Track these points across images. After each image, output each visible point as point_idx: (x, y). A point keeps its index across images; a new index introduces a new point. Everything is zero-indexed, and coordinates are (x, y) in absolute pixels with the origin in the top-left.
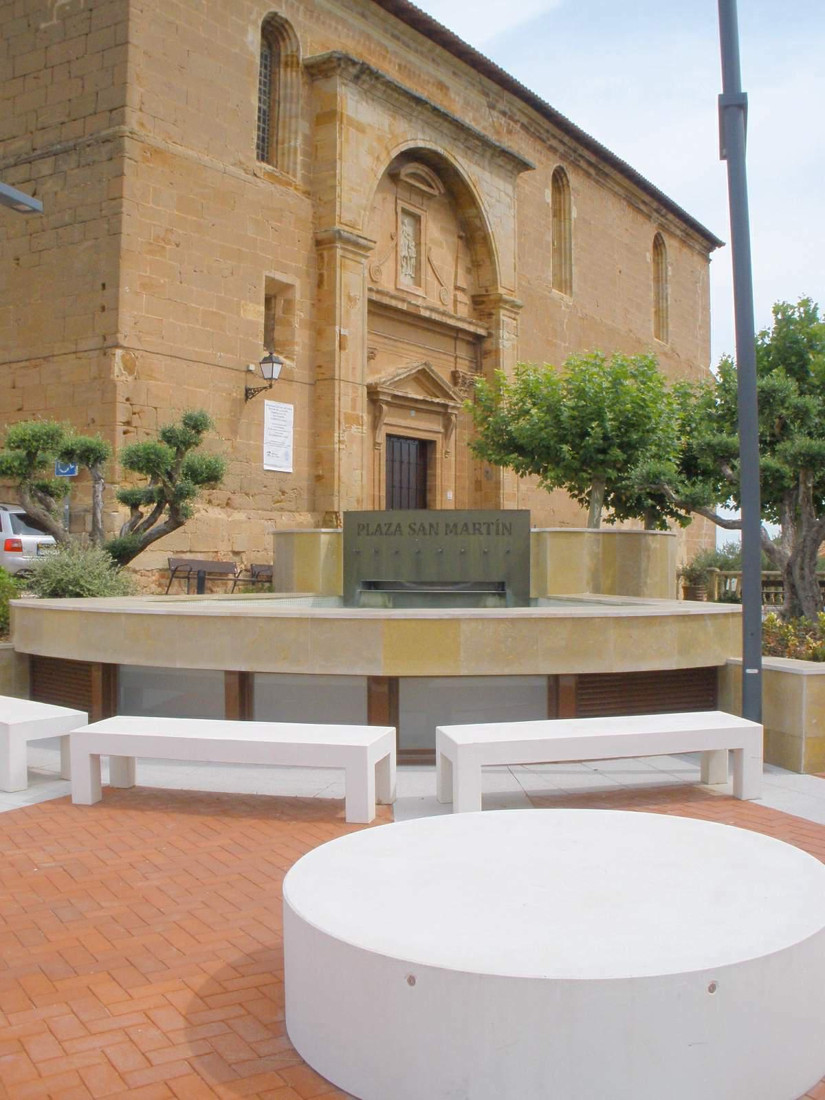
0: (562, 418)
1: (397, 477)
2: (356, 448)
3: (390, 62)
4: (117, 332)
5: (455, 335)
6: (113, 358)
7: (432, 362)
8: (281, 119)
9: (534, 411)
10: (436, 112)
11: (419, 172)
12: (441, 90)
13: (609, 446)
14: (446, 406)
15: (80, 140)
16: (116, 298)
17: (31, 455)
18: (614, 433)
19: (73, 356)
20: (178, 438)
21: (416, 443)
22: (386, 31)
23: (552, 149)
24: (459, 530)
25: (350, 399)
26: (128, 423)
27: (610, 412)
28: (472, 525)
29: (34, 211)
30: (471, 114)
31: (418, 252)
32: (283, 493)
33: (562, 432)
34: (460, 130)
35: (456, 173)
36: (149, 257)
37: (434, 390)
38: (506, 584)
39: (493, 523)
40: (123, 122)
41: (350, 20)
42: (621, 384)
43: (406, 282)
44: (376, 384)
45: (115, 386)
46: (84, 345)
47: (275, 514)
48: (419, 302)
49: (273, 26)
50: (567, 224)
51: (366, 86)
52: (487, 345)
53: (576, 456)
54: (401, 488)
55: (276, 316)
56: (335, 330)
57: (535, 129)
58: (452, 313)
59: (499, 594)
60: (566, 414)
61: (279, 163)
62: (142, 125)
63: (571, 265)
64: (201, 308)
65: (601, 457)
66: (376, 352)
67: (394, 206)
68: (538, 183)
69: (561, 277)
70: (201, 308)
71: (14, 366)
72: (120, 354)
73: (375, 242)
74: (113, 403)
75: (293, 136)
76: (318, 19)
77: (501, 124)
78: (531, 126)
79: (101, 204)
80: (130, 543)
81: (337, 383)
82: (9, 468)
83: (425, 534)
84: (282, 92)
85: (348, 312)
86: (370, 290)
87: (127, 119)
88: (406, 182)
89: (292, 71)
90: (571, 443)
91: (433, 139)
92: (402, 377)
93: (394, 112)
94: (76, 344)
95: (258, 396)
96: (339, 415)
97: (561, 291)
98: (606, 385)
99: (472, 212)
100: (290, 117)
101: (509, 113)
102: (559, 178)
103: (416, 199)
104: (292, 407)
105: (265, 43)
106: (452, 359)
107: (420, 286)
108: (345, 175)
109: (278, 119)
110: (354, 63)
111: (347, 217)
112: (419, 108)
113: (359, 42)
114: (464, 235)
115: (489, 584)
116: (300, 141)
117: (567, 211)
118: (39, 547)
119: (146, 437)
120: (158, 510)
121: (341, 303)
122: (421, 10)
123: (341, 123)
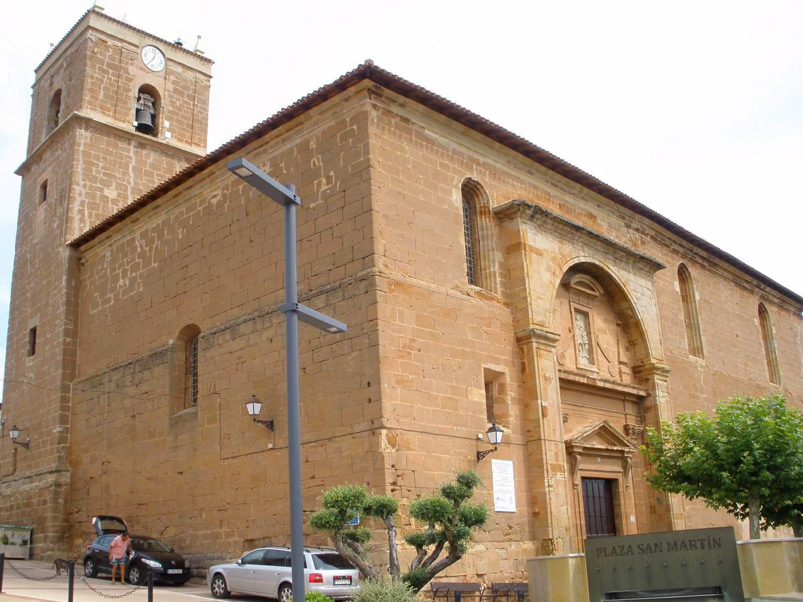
0: (719, 452)
1: (592, 509)
2: (561, 490)
3: (553, 203)
4: (382, 417)
5: (623, 398)
6: (380, 437)
7: (609, 419)
8: (482, 253)
9: (696, 449)
10: (590, 235)
11: (583, 280)
12: (591, 219)
13: (760, 470)
14: (622, 452)
15: (344, 281)
16: (379, 392)
17: (342, 512)
18: (761, 459)
19: (350, 436)
20: (455, 493)
21: (603, 481)
22: (547, 181)
23: (675, 251)
24: (679, 547)
25: (553, 454)
26: (394, 484)
27: (757, 443)
28: (688, 542)
29: (340, 331)
30: (614, 234)
31: (590, 340)
32: (511, 527)
33: (720, 462)
34: (609, 246)
35: (610, 277)
36: (400, 360)
37: (613, 441)
38: (723, 588)
39: (705, 540)
40: (374, 266)
41: (522, 177)
42: (762, 421)
43: (583, 362)
44: (570, 440)
45: (383, 457)
46: (357, 428)
47: (506, 544)
48: (595, 376)
49: (468, 187)
50: (693, 305)
51: (539, 222)
52: (648, 403)
53: (733, 480)
54: (595, 517)
55: (494, 397)
56: (538, 403)
57: (661, 238)
58: (619, 381)
59: (718, 597)
60: (721, 448)
61: (484, 284)
62: (386, 266)
63: (700, 335)
64: (440, 395)
65: (754, 479)
66: (567, 417)
67: (568, 307)
68: (669, 278)
69: (694, 346)
70: (440, 395)
71: (306, 446)
72: (385, 433)
73: (560, 335)
74: (383, 469)
75: (492, 264)
76: (499, 179)
77: (636, 238)
78: (658, 236)
79: (362, 325)
80: (421, 574)
81: (543, 442)
82: (328, 522)
83: (651, 552)
84: (480, 233)
85: (545, 388)
86: (560, 371)
87: (376, 263)
88: (576, 289)
89: (485, 217)
90: (728, 470)
91: (591, 255)
92: (589, 433)
93: (561, 238)
94: (352, 428)
95: (487, 457)
96: (547, 466)
97: (696, 356)
98: (749, 422)
99: (624, 305)
100: (488, 251)
101: (641, 230)
102: (683, 273)
103: (584, 300)
104: (511, 463)
105: (465, 200)
106: (623, 416)
107: (594, 364)
108: (532, 288)
109: (480, 253)
110: (529, 207)
111: (537, 318)
112: (579, 234)
113: (529, 192)
114: (621, 323)
115: (710, 588)
116: (497, 267)
117: (692, 296)
118: (336, 578)
119: (431, 494)
120: (439, 547)
121: (540, 383)
122: (570, 164)
123: (525, 251)
